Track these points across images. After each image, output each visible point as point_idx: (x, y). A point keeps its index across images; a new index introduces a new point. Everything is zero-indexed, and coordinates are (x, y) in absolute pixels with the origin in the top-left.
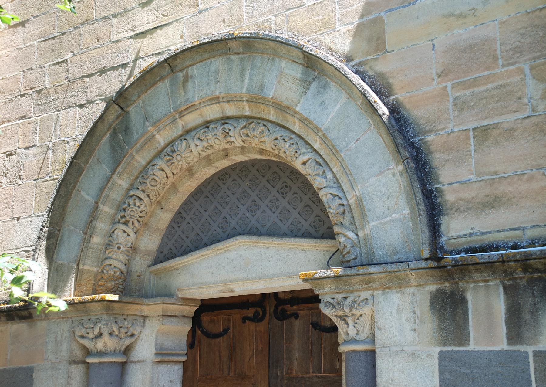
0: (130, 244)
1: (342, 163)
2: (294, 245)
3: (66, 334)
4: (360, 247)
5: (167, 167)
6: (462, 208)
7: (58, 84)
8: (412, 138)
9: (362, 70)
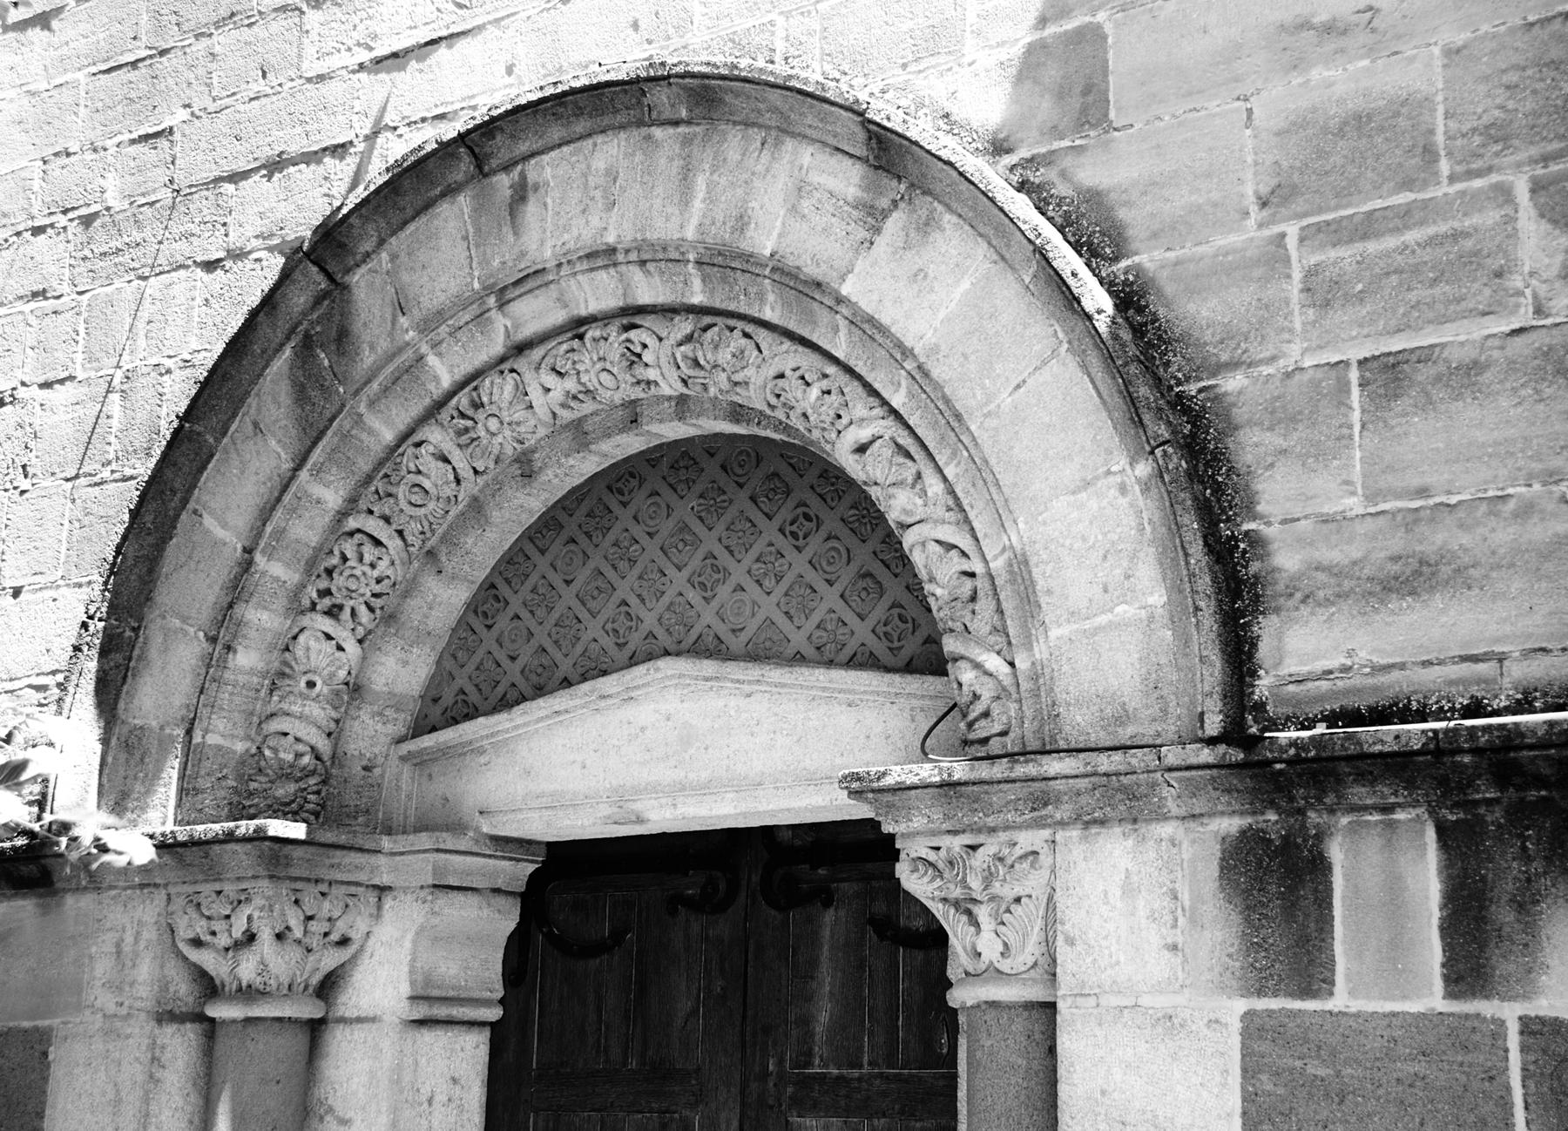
0: (342, 674)
1: (972, 451)
2: (824, 689)
3: (150, 934)
4: (1020, 701)
5: (458, 451)
6: (1321, 594)
7: (143, 201)
8: (1179, 383)
9: (1037, 181)
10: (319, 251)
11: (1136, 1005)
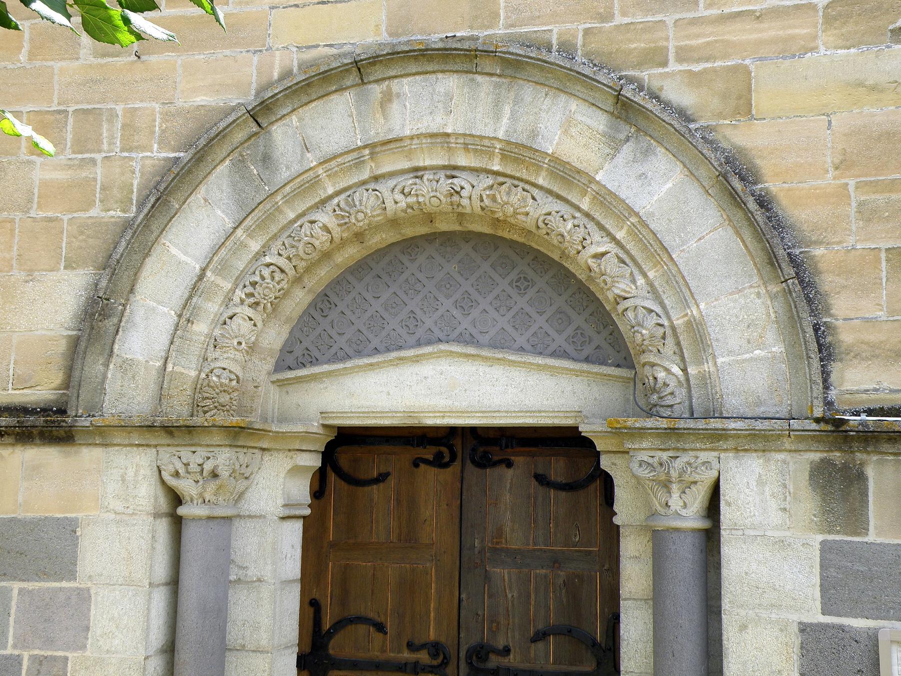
6: (864, 355)
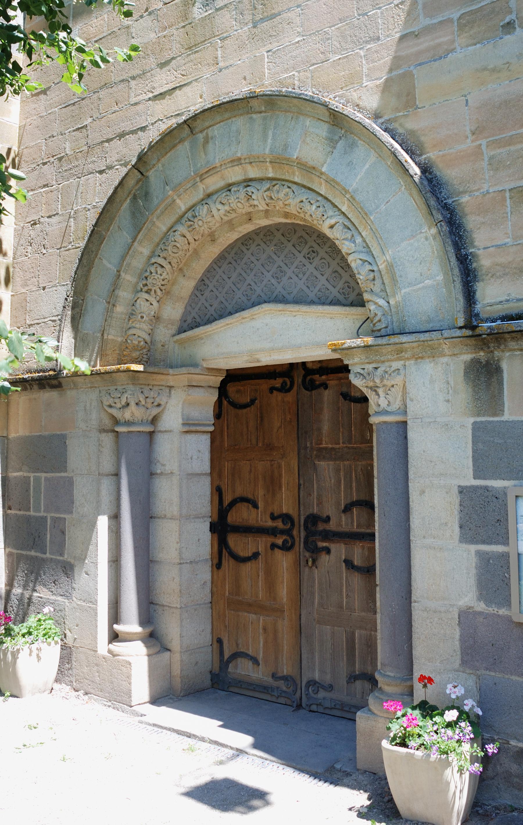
0: (153, 313)
1: (372, 226)
2: (322, 313)
3: (95, 404)
4: (392, 316)
5: (188, 233)
6: (498, 274)
7: (78, 151)
8: (445, 200)
9: (391, 128)
10: (138, 165)
11: (435, 421)
